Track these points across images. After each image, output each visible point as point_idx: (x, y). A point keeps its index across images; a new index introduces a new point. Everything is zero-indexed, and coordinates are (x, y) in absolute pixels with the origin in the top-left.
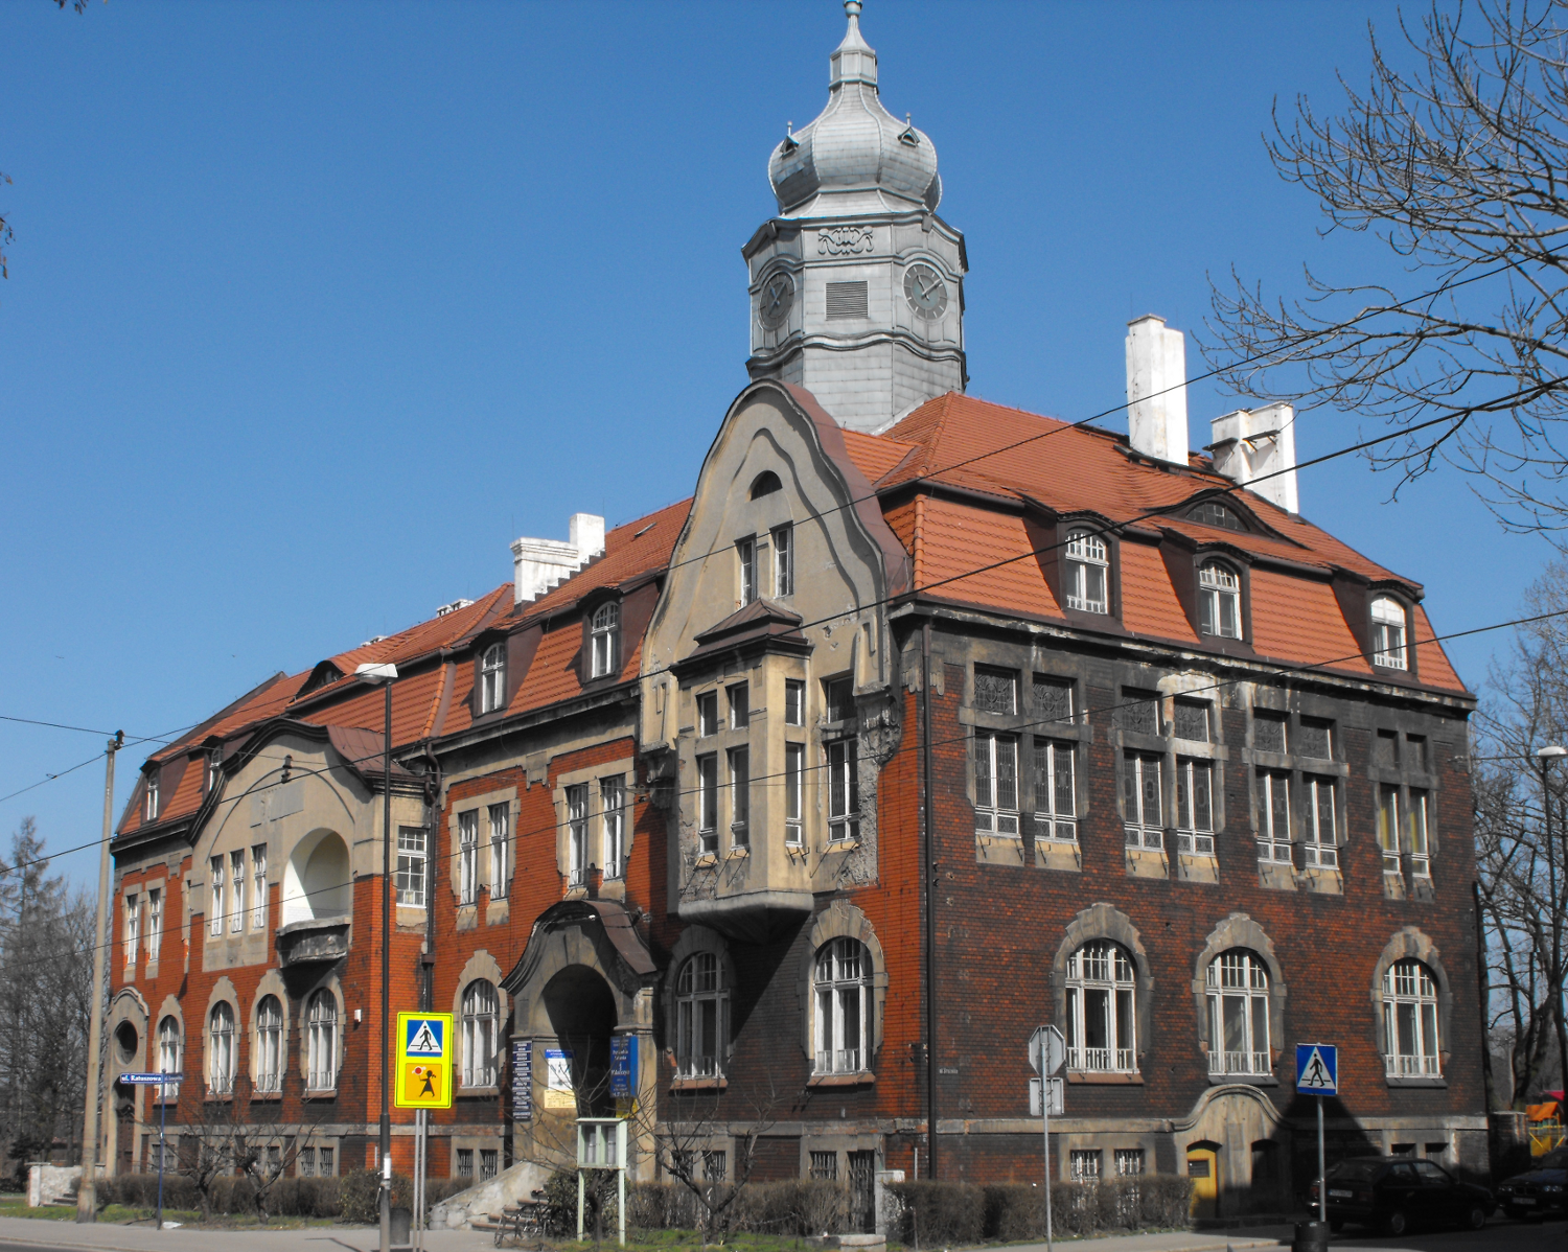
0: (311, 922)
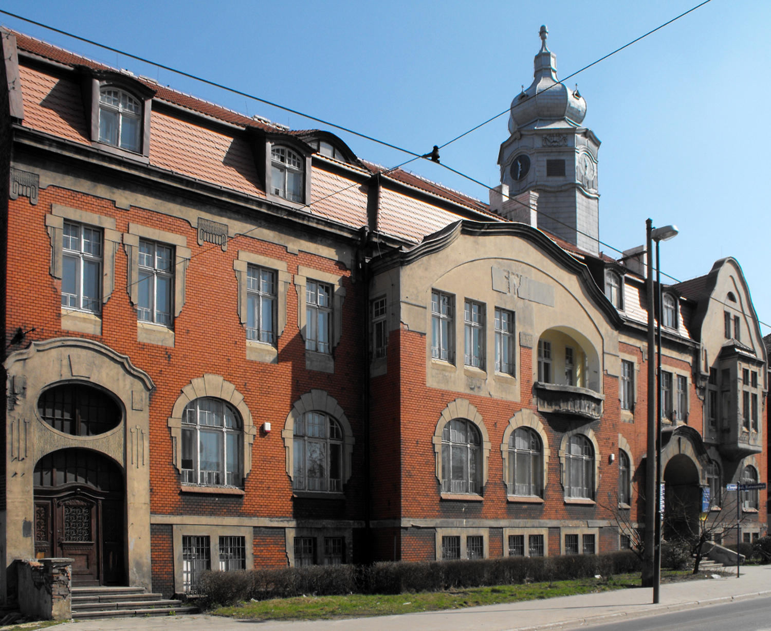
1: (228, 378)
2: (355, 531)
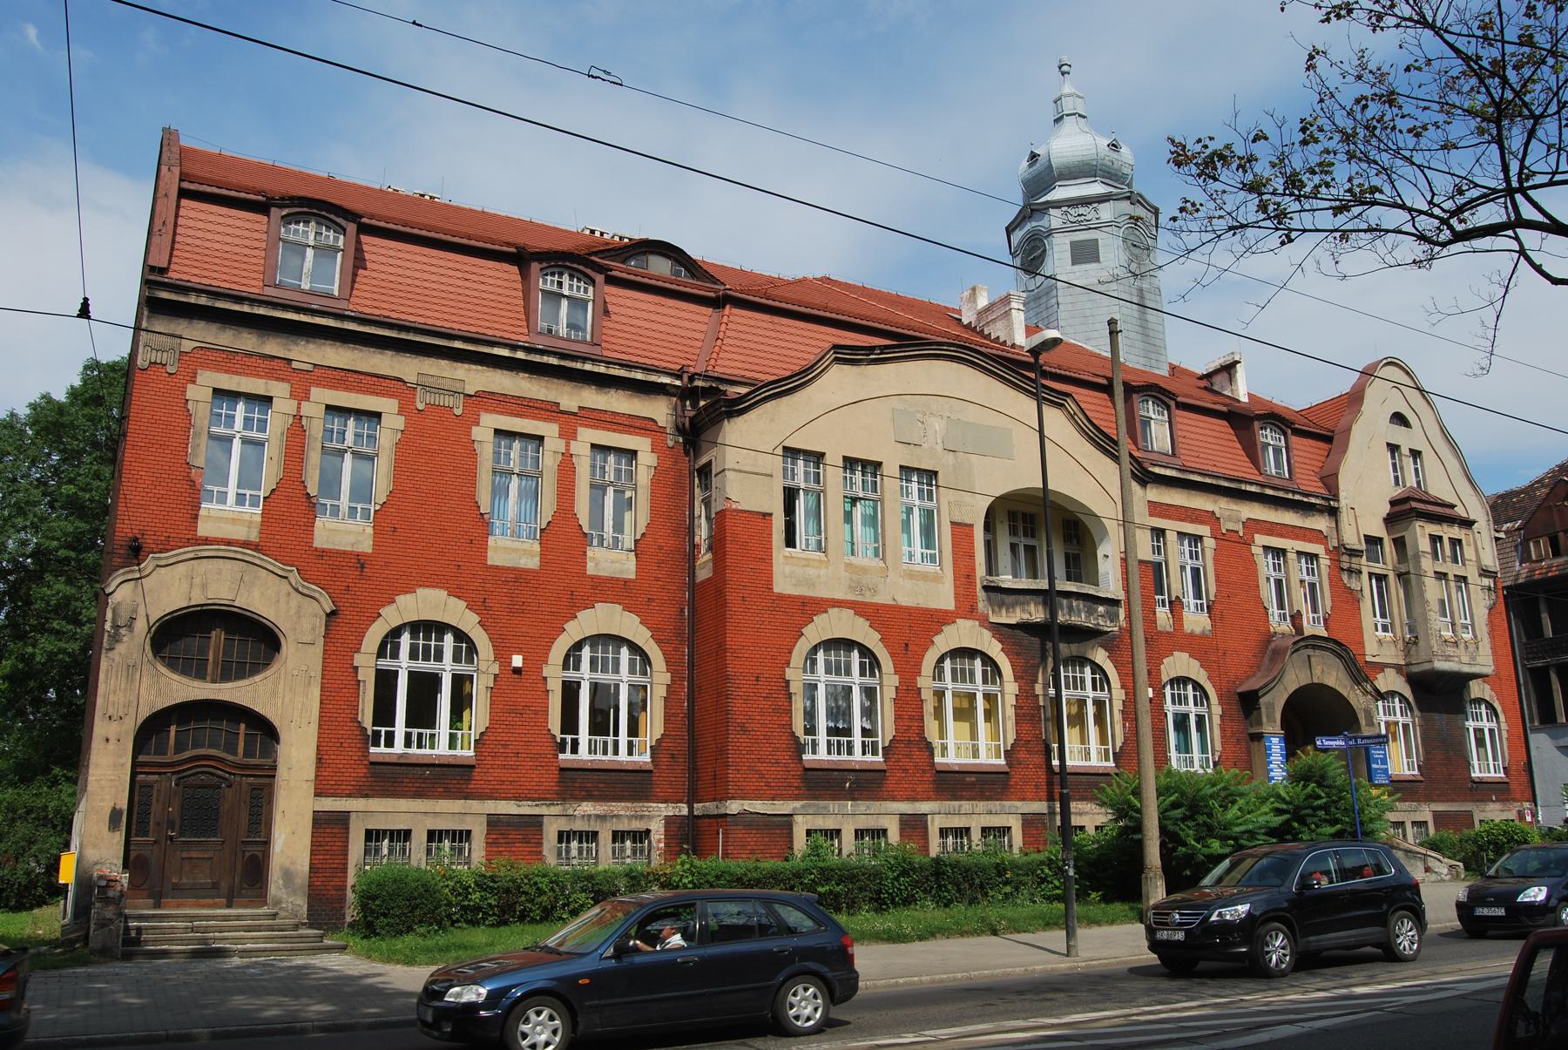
1: (456, 592)
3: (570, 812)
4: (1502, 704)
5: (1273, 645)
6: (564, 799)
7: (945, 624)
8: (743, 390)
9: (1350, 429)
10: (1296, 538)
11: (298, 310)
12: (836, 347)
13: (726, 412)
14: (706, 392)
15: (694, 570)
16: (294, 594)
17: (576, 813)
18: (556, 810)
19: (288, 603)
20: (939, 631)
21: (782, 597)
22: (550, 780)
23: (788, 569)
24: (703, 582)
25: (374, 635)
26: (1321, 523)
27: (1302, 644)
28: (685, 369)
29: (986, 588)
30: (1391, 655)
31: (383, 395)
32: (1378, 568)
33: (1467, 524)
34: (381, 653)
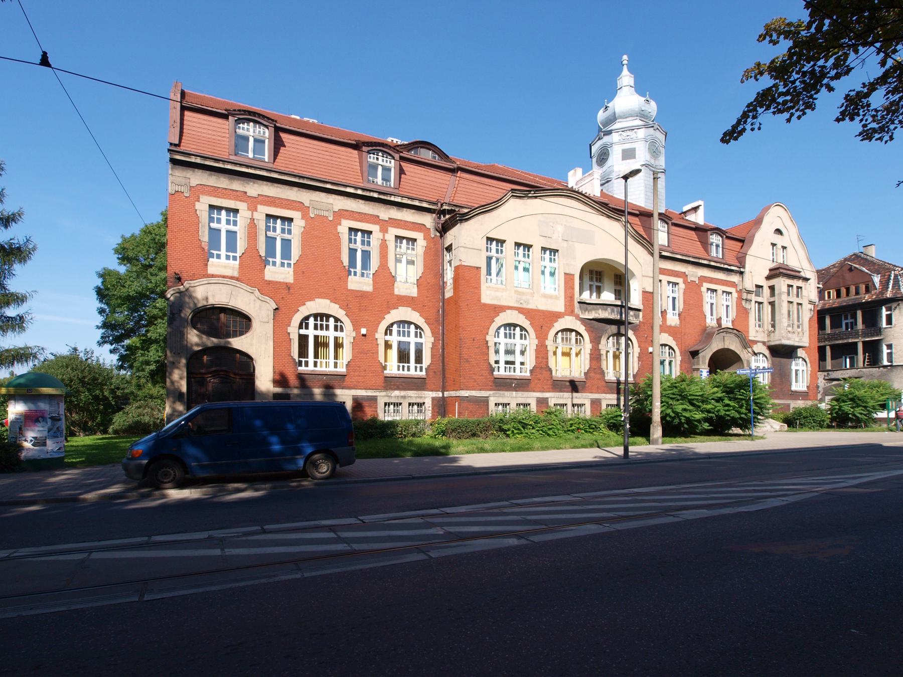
0: (613, 301)
1: (334, 300)
2: (433, 399)
3: (389, 395)
4: (810, 359)
5: (707, 331)
6: (387, 389)
7: (559, 318)
8: (466, 211)
9: (754, 236)
10: (723, 285)
11: (248, 167)
12: (512, 190)
13: (459, 220)
14: (449, 212)
15: (444, 293)
16: (258, 301)
17: (392, 395)
18: (383, 394)
19: (255, 304)
20: (556, 321)
21: (485, 305)
22: (380, 381)
23: (488, 292)
24: (448, 298)
25: (297, 319)
26: (735, 278)
27: (722, 331)
28: (439, 201)
29: (579, 303)
30: (762, 337)
31: (294, 210)
32: (760, 299)
33: (806, 280)
34: (300, 327)
